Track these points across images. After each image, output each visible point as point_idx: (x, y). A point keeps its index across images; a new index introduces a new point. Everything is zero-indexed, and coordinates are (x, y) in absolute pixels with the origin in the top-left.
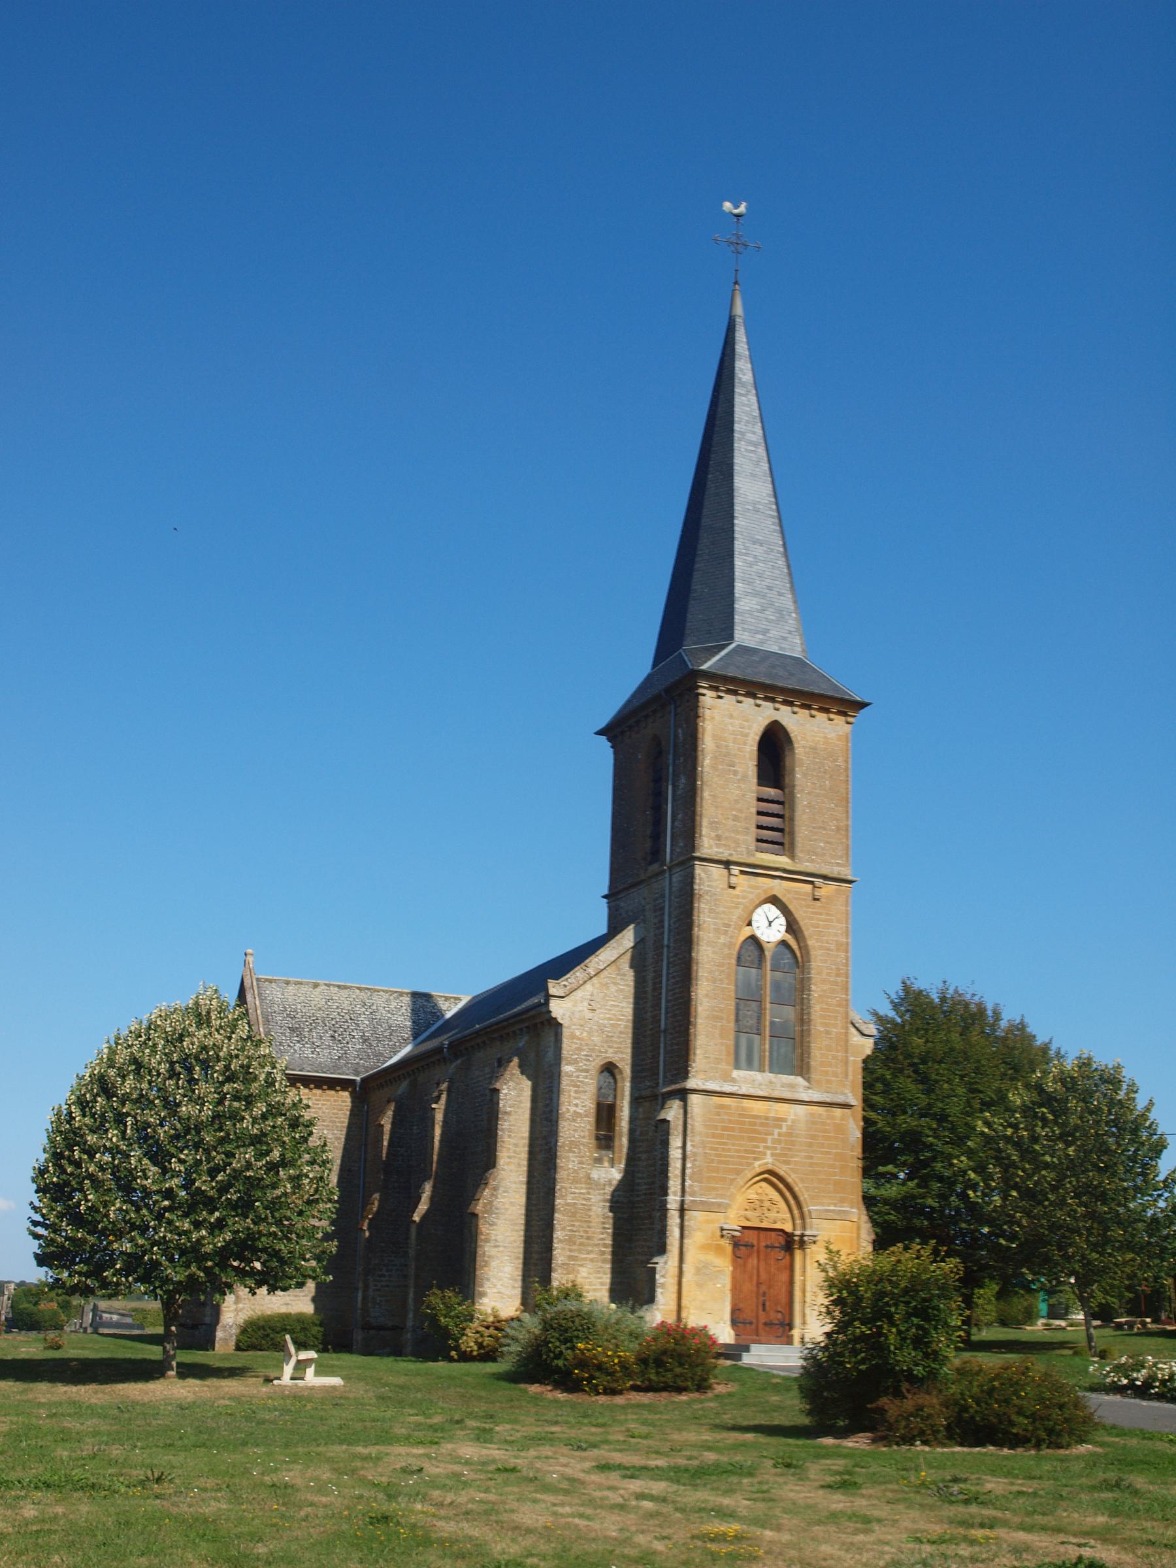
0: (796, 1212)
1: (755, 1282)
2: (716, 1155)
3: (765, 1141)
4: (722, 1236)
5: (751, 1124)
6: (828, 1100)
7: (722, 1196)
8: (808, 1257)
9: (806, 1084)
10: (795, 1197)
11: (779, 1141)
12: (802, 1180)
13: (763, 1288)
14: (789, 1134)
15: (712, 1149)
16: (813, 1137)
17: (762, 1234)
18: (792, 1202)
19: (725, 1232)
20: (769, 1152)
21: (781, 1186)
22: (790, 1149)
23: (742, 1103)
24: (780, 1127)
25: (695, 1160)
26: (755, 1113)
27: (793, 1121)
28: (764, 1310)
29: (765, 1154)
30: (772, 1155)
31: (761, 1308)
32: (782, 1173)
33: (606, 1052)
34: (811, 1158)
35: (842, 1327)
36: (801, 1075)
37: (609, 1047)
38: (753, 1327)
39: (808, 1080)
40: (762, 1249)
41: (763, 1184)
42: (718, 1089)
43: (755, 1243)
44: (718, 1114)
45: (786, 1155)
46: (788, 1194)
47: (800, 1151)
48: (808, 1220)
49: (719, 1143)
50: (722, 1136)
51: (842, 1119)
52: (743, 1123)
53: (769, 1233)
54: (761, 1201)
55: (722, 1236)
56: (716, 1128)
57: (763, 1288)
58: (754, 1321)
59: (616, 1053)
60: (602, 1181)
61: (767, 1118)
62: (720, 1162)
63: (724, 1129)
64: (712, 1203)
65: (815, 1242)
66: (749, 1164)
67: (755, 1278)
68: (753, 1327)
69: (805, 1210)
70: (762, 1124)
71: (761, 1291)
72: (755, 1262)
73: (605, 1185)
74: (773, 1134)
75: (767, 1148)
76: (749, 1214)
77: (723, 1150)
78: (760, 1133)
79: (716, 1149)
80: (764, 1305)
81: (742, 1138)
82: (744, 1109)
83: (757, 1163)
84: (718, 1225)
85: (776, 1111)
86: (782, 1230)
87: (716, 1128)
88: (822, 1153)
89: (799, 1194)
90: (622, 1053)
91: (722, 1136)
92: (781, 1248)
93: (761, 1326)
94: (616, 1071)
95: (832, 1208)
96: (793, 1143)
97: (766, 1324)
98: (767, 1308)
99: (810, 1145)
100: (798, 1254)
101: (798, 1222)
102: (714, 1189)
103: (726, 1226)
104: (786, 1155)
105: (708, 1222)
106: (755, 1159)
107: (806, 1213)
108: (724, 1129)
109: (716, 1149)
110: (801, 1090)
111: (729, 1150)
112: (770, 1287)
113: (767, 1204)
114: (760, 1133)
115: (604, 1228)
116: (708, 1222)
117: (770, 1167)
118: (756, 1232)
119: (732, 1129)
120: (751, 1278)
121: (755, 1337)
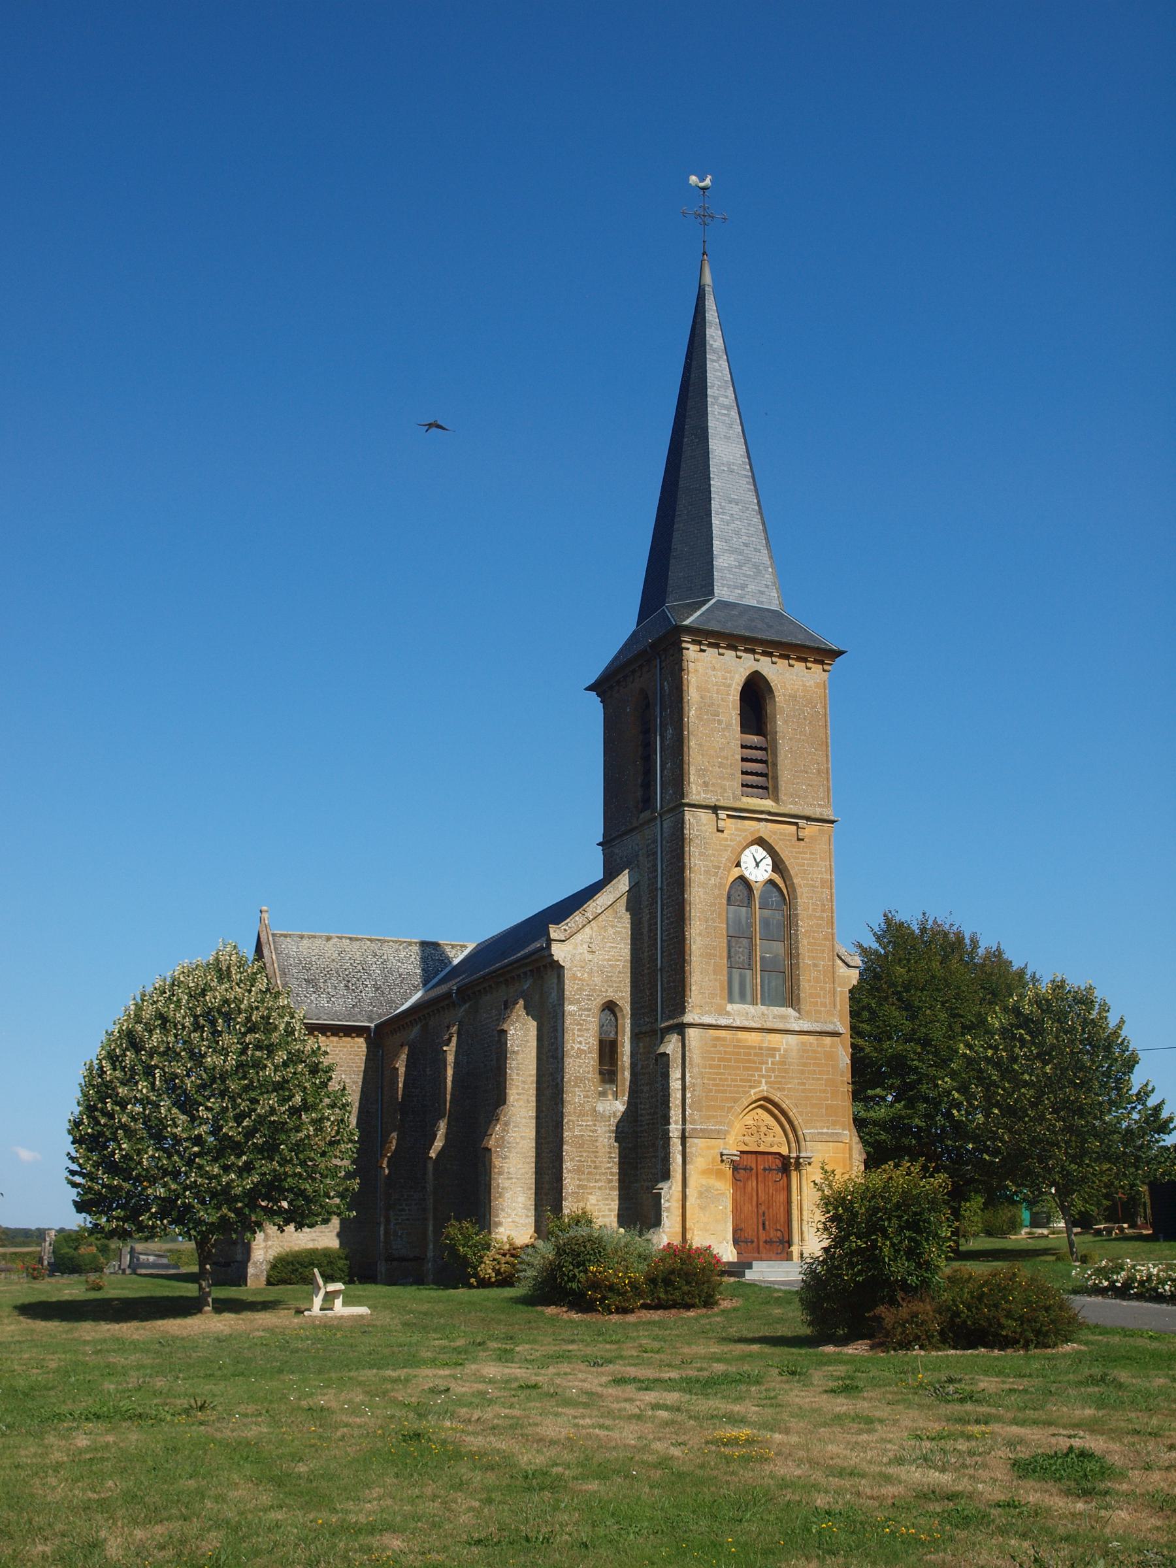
1: (754, 1203)
3: (761, 1070)
6: (818, 1029)
7: (720, 1123)
9: (797, 1015)
11: (773, 1070)
13: (762, 1208)
14: (783, 1063)
15: (709, 1079)
16: (805, 1065)
18: (787, 1126)
20: (763, 1080)
22: (784, 1077)
24: (774, 1056)
27: (786, 1050)
28: (764, 1228)
29: (760, 1082)
30: (767, 1083)
31: (761, 1227)
34: (804, 1084)
35: (838, 1242)
37: (609, 986)
39: (799, 1011)
40: (760, 1171)
41: (759, 1111)
42: (714, 1022)
43: (754, 1166)
45: (780, 1083)
47: (793, 1078)
51: (831, 1047)
53: (766, 1156)
56: (713, 1059)
57: (762, 1208)
61: (761, 1048)
62: (718, 1091)
63: (720, 1060)
65: (810, 1164)
68: (755, 1244)
69: (800, 1133)
71: (761, 1211)
72: (754, 1184)
74: (767, 1063)
75: (763, 1076)
77: (720, 1079)
79: (714, 1079)
81: (738, 1068)
82: (739, 1040)
83: (753, 1091)
87: (713, 1059)
90: (621, 991)
92: (778, 1170)
93: (761, 1243)
94: (617, 1010)
95: (825, 1131)
97: (766, 1242)
98: (767, 1227)
99: (802, 1072)
100: (794, 1175)
102: (713, 1116)
104: (780, 1083)
105: (709, 1148)
106: (751, 1087)
108: (720, 1060)
109: (714, 1079)
110: (793, 1020)
111: (726, 1080)
115: (611, 1157)
116: (709, 1148)
117: (765, 1094)
118: (754, 1156)
119: (729, 1060)
121: (756, 1255)
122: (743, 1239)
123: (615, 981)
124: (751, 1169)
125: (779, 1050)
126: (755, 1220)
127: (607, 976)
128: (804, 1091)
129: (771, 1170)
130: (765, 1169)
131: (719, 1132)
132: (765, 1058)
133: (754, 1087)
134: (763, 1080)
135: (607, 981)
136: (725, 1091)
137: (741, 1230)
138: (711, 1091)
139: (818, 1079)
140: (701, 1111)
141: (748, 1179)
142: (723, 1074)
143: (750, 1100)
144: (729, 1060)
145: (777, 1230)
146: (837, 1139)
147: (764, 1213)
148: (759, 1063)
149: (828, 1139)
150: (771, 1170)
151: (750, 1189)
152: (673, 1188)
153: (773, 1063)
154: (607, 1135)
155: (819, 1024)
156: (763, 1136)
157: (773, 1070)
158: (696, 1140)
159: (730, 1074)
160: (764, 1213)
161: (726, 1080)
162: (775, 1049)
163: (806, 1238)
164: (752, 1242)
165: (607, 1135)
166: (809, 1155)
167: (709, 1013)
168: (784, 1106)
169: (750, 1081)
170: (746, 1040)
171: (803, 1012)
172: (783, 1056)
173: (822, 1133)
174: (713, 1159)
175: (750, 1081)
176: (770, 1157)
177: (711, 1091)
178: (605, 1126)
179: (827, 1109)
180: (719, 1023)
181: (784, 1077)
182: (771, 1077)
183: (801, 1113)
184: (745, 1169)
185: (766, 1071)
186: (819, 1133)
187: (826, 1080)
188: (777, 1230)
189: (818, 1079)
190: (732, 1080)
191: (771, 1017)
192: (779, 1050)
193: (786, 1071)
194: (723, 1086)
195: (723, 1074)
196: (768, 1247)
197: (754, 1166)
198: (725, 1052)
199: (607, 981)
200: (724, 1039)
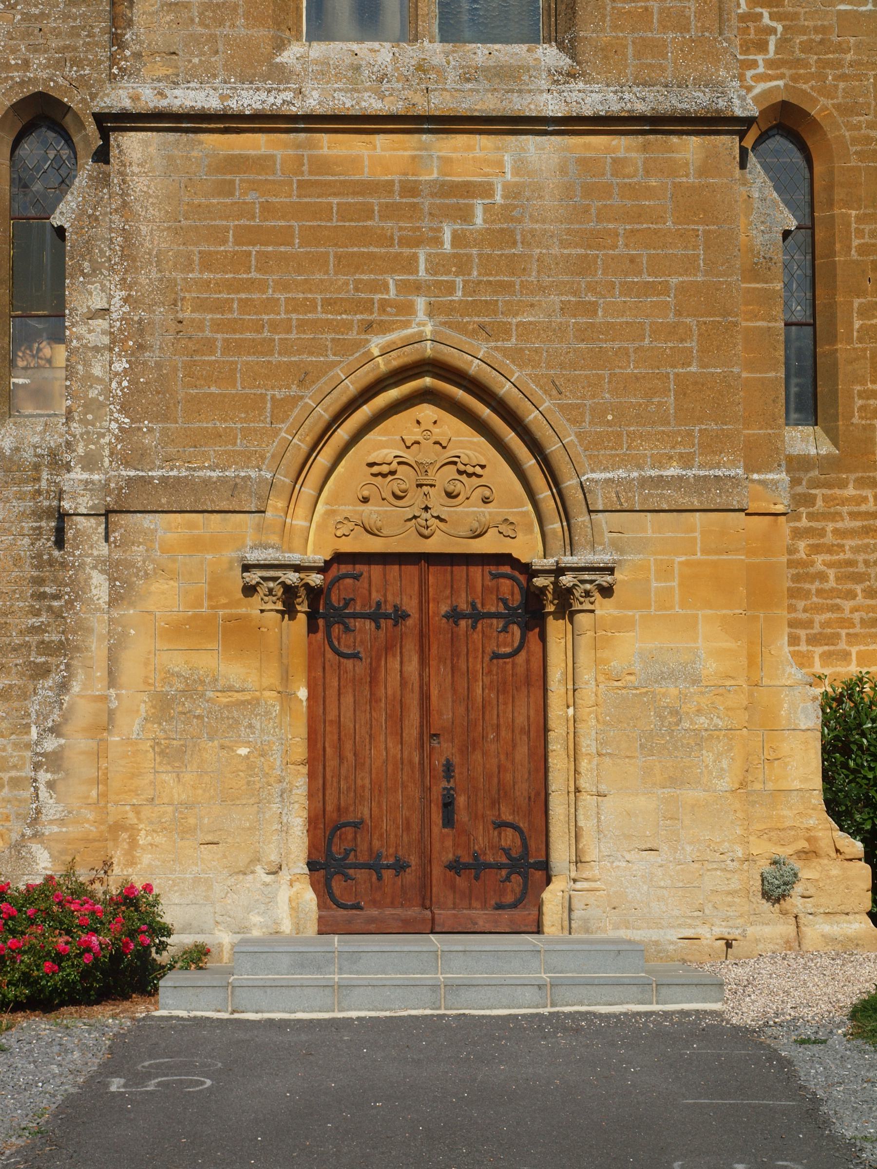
0: (545, 494)
1: (412, 732)
2: (218, 326)
3: (411, 264)
4: (249, 590)
5: (345, 212)
6: (641, 108)
7: (246, 458)
8: (584, 641)
9: (564, 62)
10: (536, 447)
11: (462, 265)
12: (555, 388)
13: (446, 750)
14: (506, 237)
15: (200, 305)
16: (593, 239)
17: (436, 575)
18: (530, 462)
19: (254, 577)
20: (421, 303)
21: (485, 412)
22: (505, 287)
23: (312, 146)
24: (466, 215)
25: (141, 347)
26: (366, 175)
27: (513, 192)
28: (449, 821)
29: (408, 309)
30: (432, 310)
31: (437, 817)
32: (474, 367)
33: (26, 64)
34: (591, 309)
35: (44, 885)
36: (554, 38)
37: (35, 49)
38: (410, 876)
39: (570, 49)
40: (438, 622)
41: (427, 412)
42: (212, 103)
43: (411, 605)
44: (225, 188)
45: (489, 307)
46: (511, 437)
47: (542, 289)
48: (581, 519)
49: (232, 286)
50: (240, 261)
51: (703, 171)
52: (324, 212)
53: (460, 571)
54: (421, 468)
55: (249, 590)
56: (218, 235)
57: (446, 750)
58: (414, 860)
59: (59, 64)
60: (28, 455)
61: (411, 189)
62: (239, 347)
63: (245, 235)
64: (206, 482)
65: (607, 591)
66: (344, 348)
67: (413, 716)
68: (410, 876)
69: (570, 483)
70: (390, 211)
71: (438, 763)
72: (412, 667)
73: (37, 467)
74: (437, 241)
75: (418, 288)
76: (372, 512)
77: (245, 304)
78: (386, 240)
79: (221, 306)
80: (448, 805)
81: (320, 262)
82: (321, 165)
83: (376, 344)
84: (230, 554)
85: (446, 161)
86: (506, 559)
87: (218, 235)
88: (628, 289)
89: (543, 432)
90: (77, 63)
91: (240, 261)
92: (509, 617)
93: (437, 871)
94: (68, 121)
95: (673, 471)
96: (513, 264)
97: (455, 867)
98: (462, 816)
99: (583, 266)
100: (555, 628)
101: (555, 526)
102: (218, 436)
103: (253, 557)
104: (489, 307)
105: (196, 545)
106: (368, 327)
107: (575, 496)
108: (245, 235)
109: (221, 306)
110: (544, 84)
111: (270, 305)
112: (468, 747)
113: (445, 477)
114: (386, 240)
115: (42, 596)
116: (196, 545)
117: (428, 350)
118: (412, 571)
119: (284, 236)
120: (397, 721)
121: (414, 912)
122: (363, 858)
123: (57, 33)
124: (400, 616)
125: (486, 190)
126: (415, 792)
127: (26, 17)
128: (582, 334)
129: (476, 616)
130: (454, 616)
131: (235, 487)
132: (426, 224)
133: (384, 328)
134: (421, 303)
135: (27, 34)
136: (264, 347)
137: (357, 825)
138: (209, 345)
139: (649, 288)
140: (165, 417)
141: (388, 648)
142: (262, 286)
143: (365, 376)
144: (284, 236)
145: (501, 825)
146: (720, 502)
147: (449, 769)
148: (404, 242)
149: (684, 502)
150: (476, 616)
151: (394, 680)
152: (76, 687)
153: (457, 239)
154: (28, 525)
155: (650, 94)
156: (436, 498)
157: (462, 265)
158: (147, 521)
159: (285, 286)
160: (449, 769)
161: (270, 305)
162: (468, 190)
163: (591, 853)
164: (400, 867)
165: (28, 525)
166: (602, 558)
167: (191, 76)
168: (505, 389)
169: (366, 306)
170: (355, 162)
171: (587, 52)
172: (506, 213)
173: (660, 482)
174: (215, 581)
175: (366, 306)
176: (476, 572)
177: (209, 345)
178: (21, 497)
179: (682, 393)
180: (234, 105)
181: (505, 287)
182: (450, 288)
183: (573, 413)
184: (376, 616)
185: (432, 269)
186: (644, 482)
187: (682, 289)
188: (501, 825)
189: (649, 288)
190: (295, 306)
191: (452, 76)
192: (486, 190)
193: (513, 264)
194: (259, 327)
195: (262, 286)
196: (461, 882)
197: (411, 605)
198: (268, 209)
199: (27, 34)
200: (263, 163)
